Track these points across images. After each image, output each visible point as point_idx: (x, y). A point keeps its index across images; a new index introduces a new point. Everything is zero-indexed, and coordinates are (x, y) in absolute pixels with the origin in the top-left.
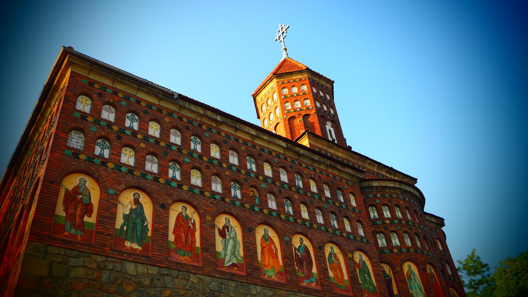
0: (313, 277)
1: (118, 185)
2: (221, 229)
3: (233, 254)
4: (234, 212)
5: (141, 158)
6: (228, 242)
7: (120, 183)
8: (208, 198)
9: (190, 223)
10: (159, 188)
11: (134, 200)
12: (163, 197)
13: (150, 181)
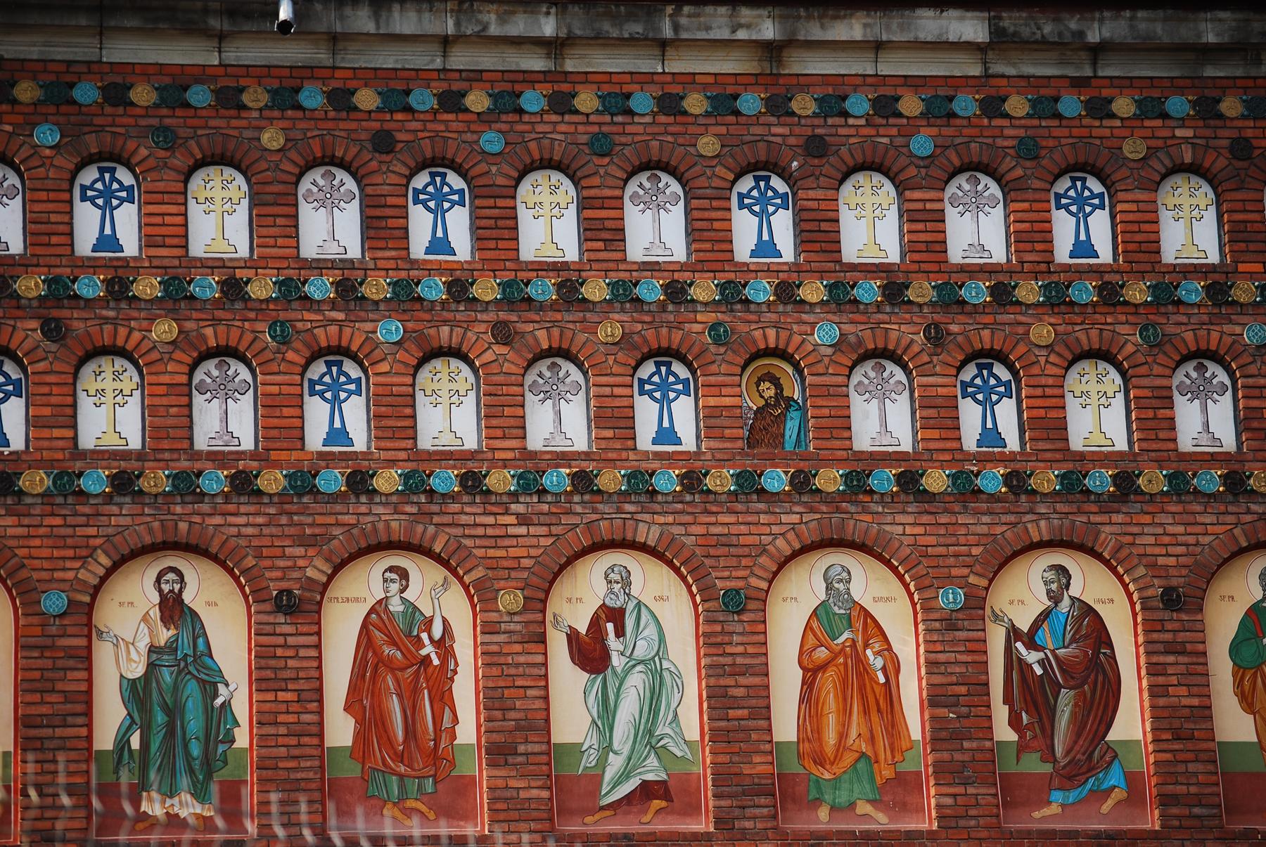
0: (1110, 763)
1: (77, 564)
2: (583, 629)
3: (647, 735)
4: (648, 533)
5: (165, 401)
6: (619, 689)
7: (84, 552)
8: (505, 499)
9: (427, 641)
10: (260, 520)
11: (160, 604)
12: (283, 556)
13: (219, 500)
